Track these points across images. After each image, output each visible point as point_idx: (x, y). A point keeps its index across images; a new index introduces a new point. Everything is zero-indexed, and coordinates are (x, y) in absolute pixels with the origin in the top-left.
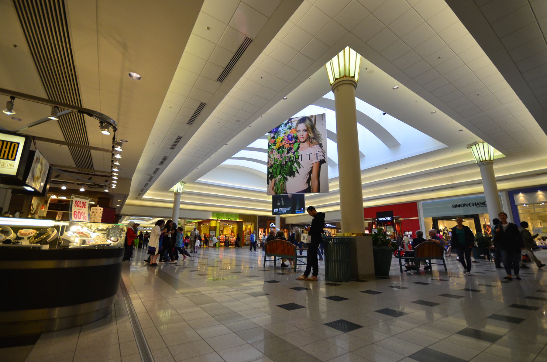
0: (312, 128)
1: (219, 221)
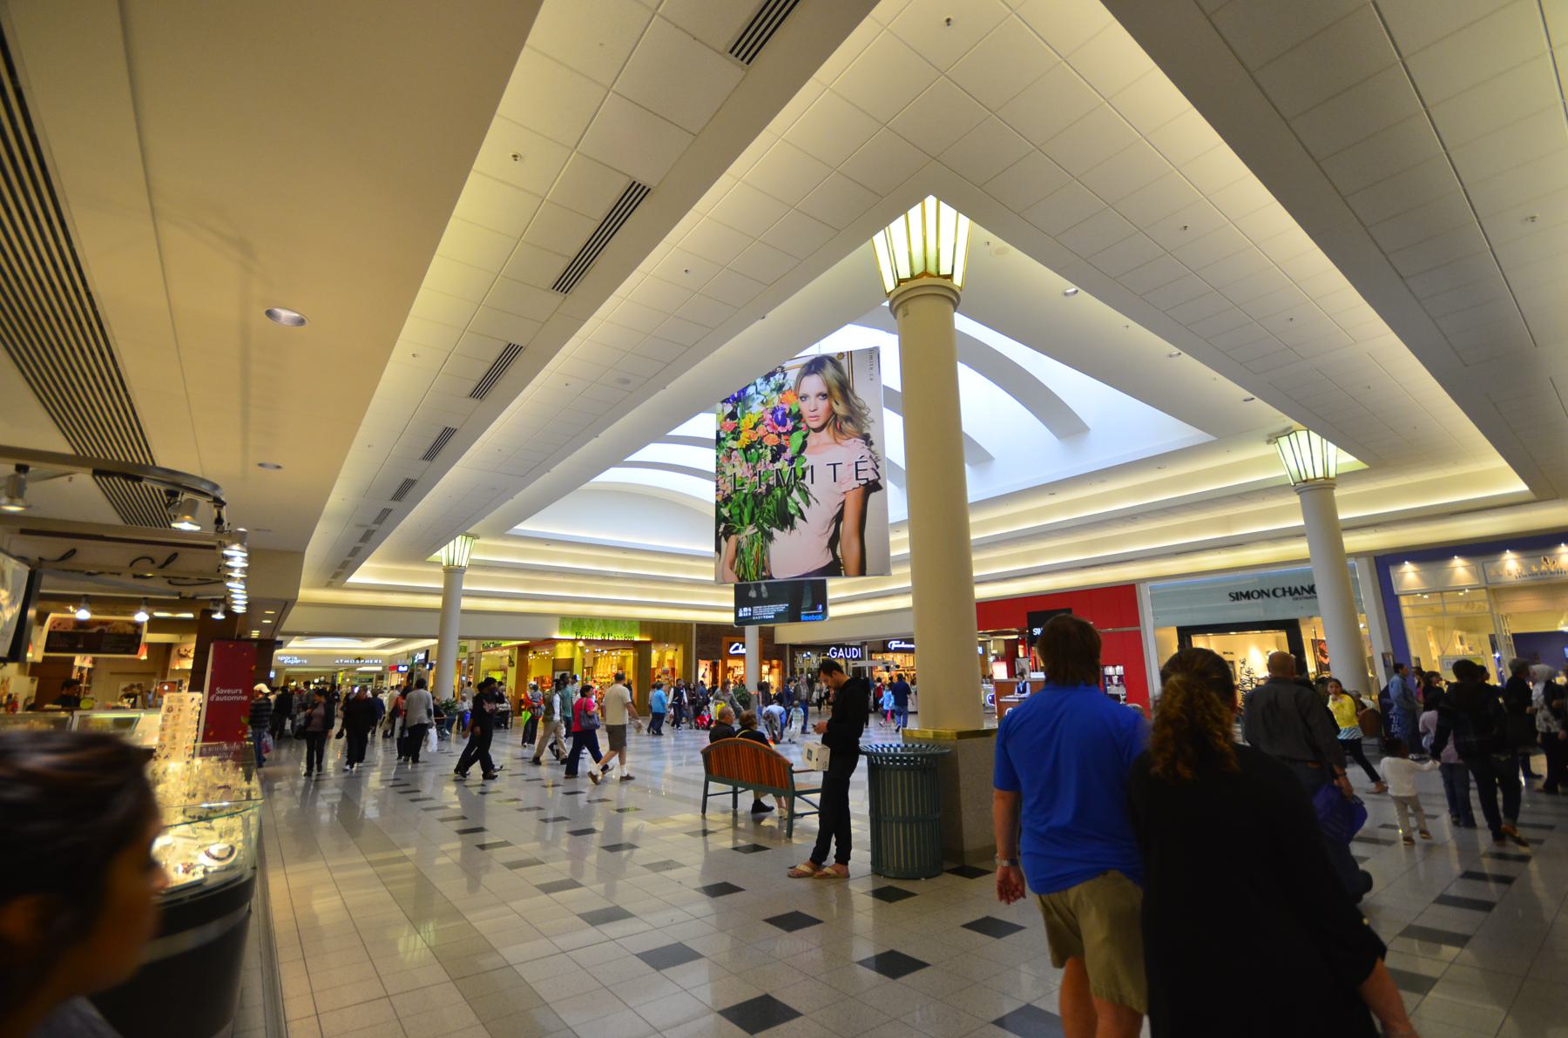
0: (843, 388)
1: (581, 644)
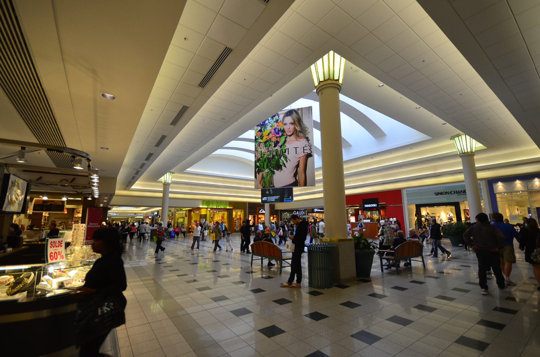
0: (299, 121)
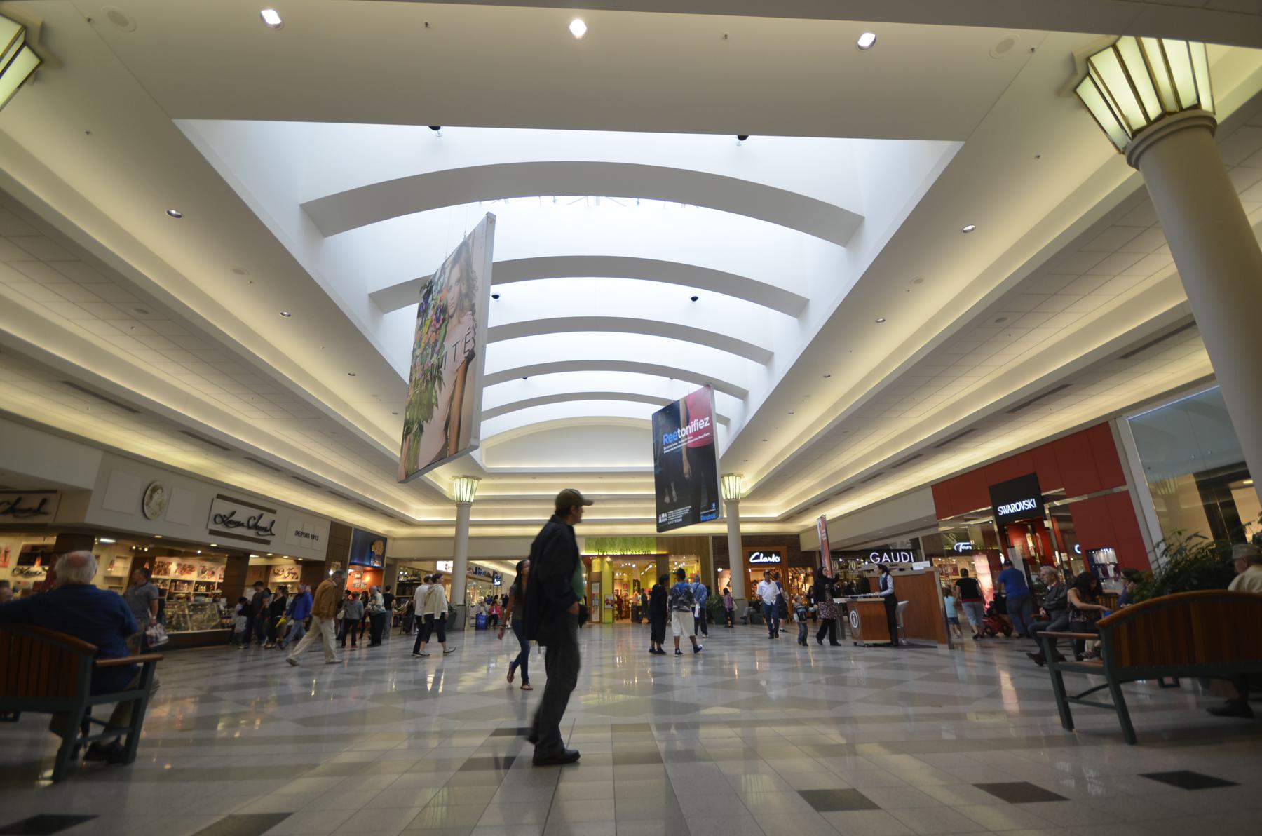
1: (608, 559)
